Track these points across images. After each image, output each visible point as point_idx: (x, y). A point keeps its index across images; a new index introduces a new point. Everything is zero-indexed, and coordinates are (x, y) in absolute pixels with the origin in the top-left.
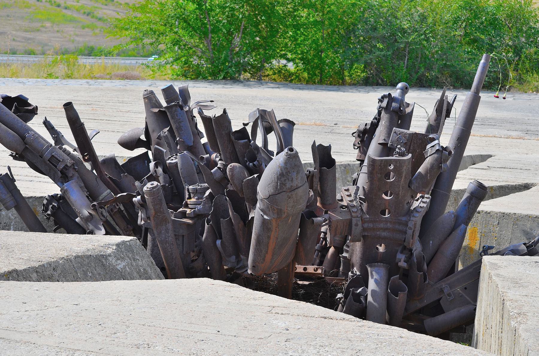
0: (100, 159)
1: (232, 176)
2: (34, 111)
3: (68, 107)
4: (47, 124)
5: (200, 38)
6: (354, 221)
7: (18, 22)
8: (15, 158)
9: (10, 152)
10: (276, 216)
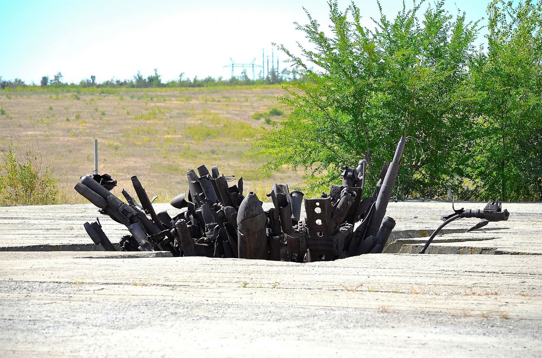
0: (157, 213)
1: (227, 213)
2: (114, 184)
3: (134, 179)
4: (124, 193)
5: (358, 153)
6: (301, 240)
7: (231, 163)
8: (101, 212)
9: (98, 209)
10: (246, 233)
